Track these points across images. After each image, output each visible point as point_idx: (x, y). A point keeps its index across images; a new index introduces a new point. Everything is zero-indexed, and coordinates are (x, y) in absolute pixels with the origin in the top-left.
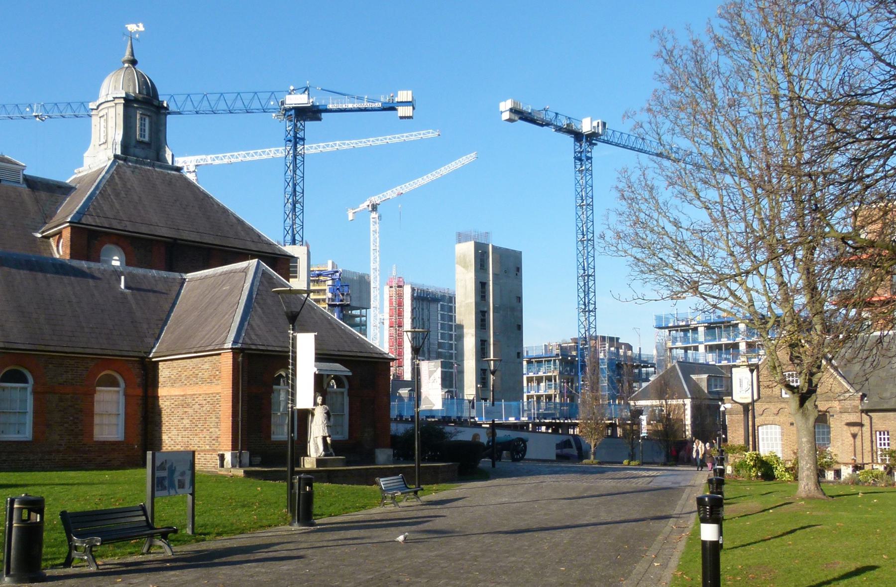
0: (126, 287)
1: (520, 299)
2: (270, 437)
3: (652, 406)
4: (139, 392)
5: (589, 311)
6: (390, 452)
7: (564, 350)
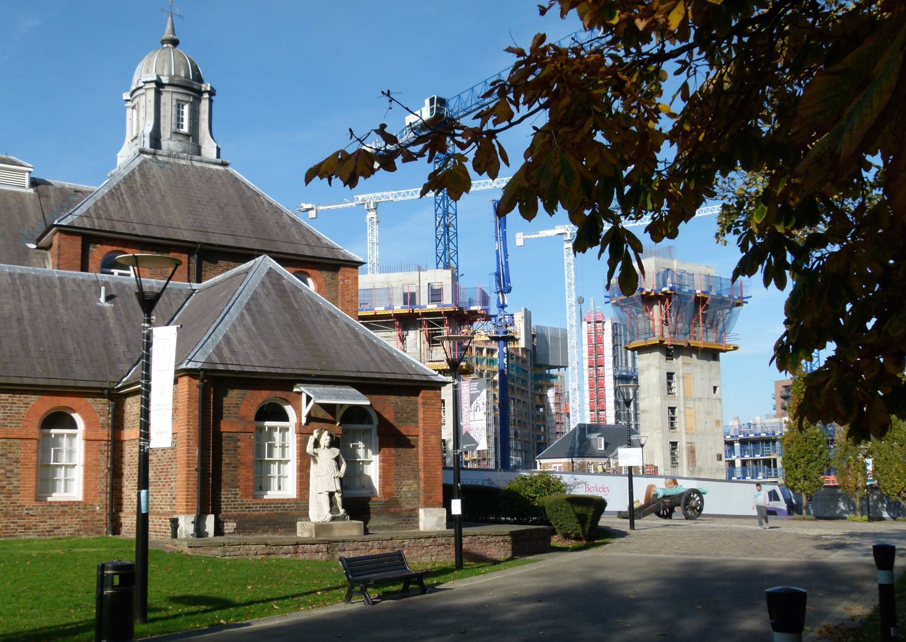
4: (104, 433)
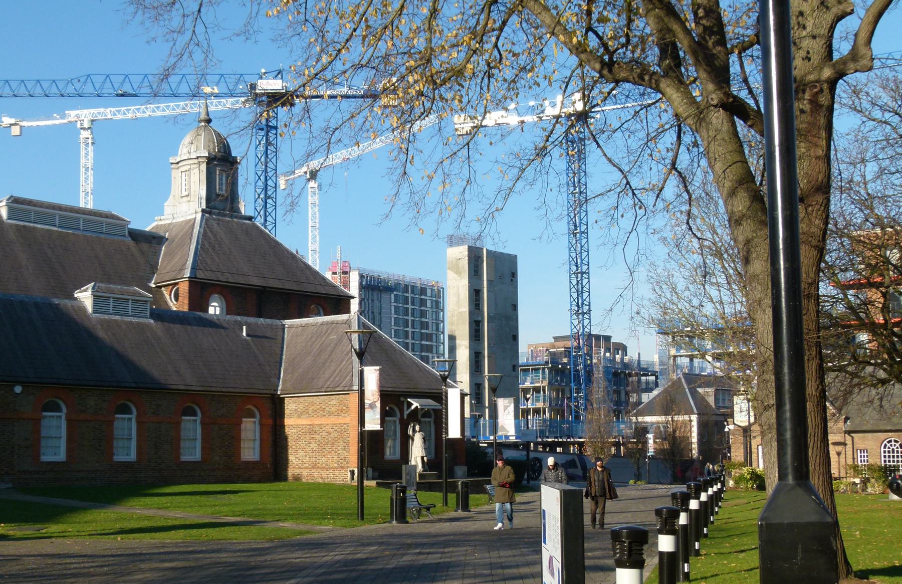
0: (248, 335)
1: (515, 307)
2: (179, 458)
3: (658, 423)
4: (270, 422)
5: (583, 314)
6: (465, 468)
7: (554, 357)
